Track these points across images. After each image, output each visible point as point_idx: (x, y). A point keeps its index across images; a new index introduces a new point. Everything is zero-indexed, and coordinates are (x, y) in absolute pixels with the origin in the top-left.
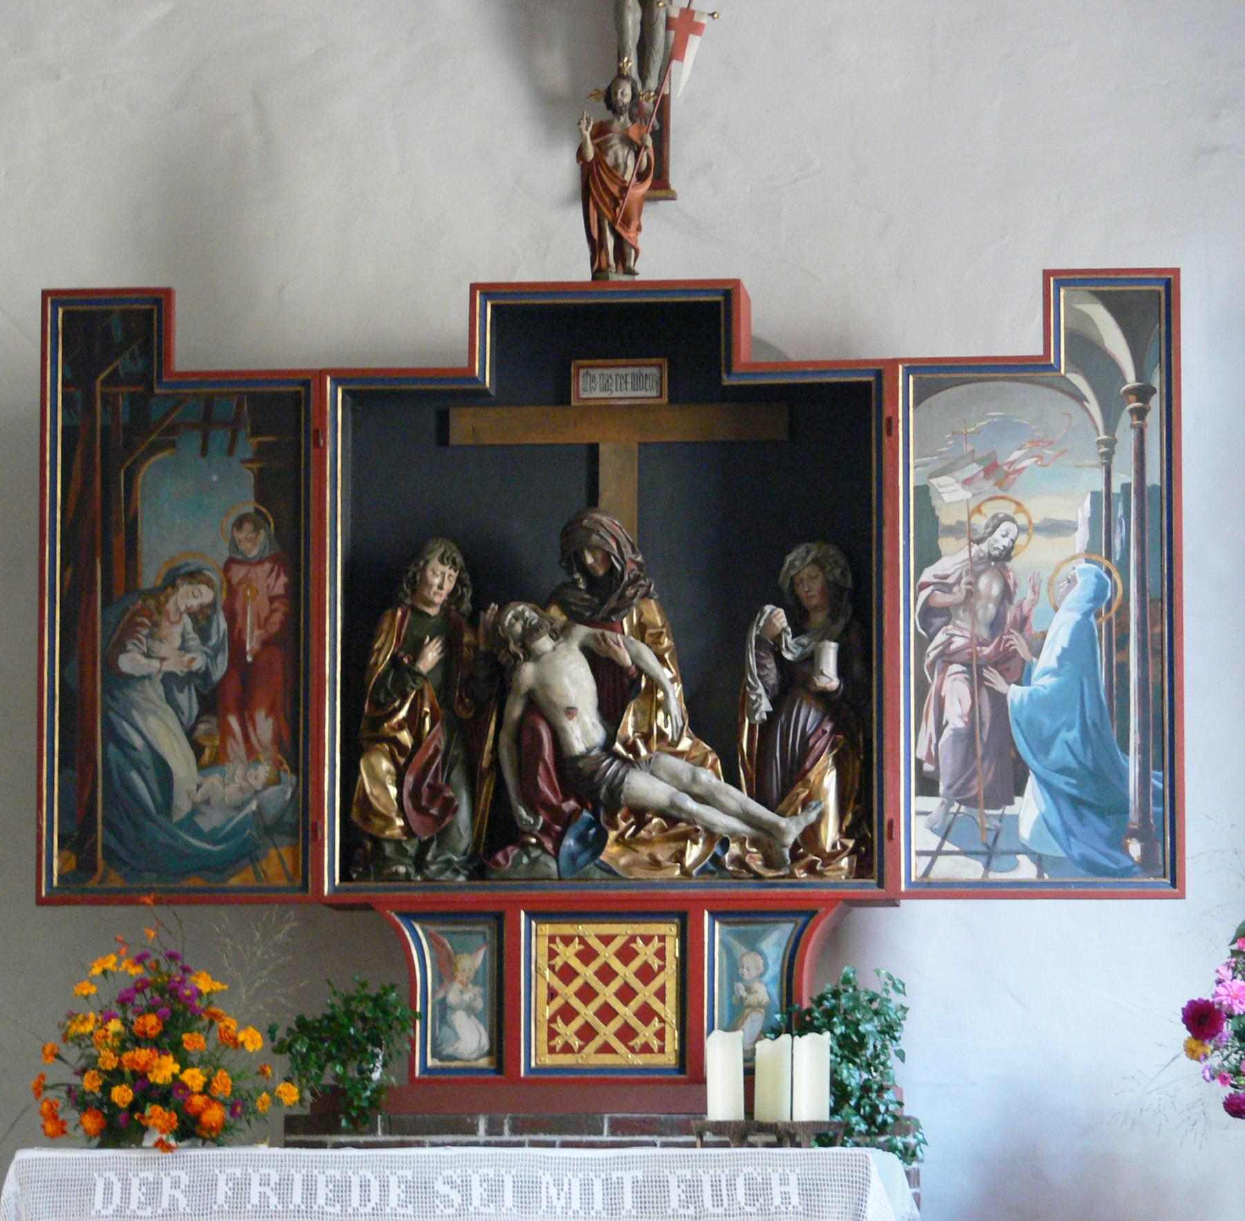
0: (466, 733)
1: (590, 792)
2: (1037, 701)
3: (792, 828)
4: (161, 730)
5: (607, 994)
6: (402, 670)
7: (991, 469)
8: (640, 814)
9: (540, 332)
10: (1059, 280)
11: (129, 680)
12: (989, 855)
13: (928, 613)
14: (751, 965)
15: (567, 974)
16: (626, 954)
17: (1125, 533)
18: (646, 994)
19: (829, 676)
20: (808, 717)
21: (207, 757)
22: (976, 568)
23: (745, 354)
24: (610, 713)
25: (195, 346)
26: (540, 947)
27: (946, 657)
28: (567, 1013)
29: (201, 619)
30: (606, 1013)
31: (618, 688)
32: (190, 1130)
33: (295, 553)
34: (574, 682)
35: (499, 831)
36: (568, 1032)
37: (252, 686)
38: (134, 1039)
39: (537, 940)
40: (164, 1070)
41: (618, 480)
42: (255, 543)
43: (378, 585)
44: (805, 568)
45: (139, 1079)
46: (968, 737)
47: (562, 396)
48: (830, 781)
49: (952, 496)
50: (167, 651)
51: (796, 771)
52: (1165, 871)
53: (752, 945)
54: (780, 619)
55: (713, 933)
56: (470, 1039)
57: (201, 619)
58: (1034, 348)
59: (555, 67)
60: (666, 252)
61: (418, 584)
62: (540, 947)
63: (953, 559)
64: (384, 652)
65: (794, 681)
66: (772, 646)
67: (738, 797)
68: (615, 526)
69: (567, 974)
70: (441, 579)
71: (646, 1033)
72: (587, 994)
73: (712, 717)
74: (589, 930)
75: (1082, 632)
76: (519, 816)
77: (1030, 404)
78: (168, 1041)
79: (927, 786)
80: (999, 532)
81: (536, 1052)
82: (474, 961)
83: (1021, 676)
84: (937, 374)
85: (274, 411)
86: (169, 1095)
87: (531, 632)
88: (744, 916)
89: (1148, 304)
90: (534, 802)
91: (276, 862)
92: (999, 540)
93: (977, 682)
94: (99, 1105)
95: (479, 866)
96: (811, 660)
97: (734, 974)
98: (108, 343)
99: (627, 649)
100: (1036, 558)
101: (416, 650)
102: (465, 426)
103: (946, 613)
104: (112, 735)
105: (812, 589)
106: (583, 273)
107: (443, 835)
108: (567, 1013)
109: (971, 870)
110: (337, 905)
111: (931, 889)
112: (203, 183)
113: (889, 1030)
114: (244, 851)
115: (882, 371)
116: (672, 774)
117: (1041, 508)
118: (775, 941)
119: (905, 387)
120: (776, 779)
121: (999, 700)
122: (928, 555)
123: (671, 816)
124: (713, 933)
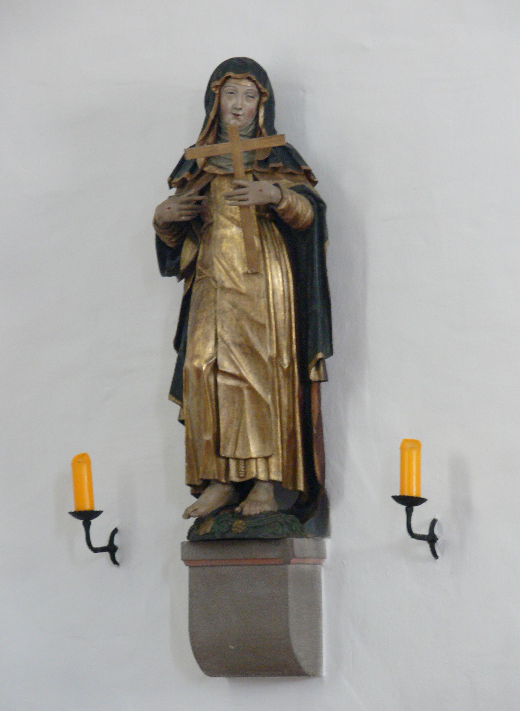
34: (277, 165)
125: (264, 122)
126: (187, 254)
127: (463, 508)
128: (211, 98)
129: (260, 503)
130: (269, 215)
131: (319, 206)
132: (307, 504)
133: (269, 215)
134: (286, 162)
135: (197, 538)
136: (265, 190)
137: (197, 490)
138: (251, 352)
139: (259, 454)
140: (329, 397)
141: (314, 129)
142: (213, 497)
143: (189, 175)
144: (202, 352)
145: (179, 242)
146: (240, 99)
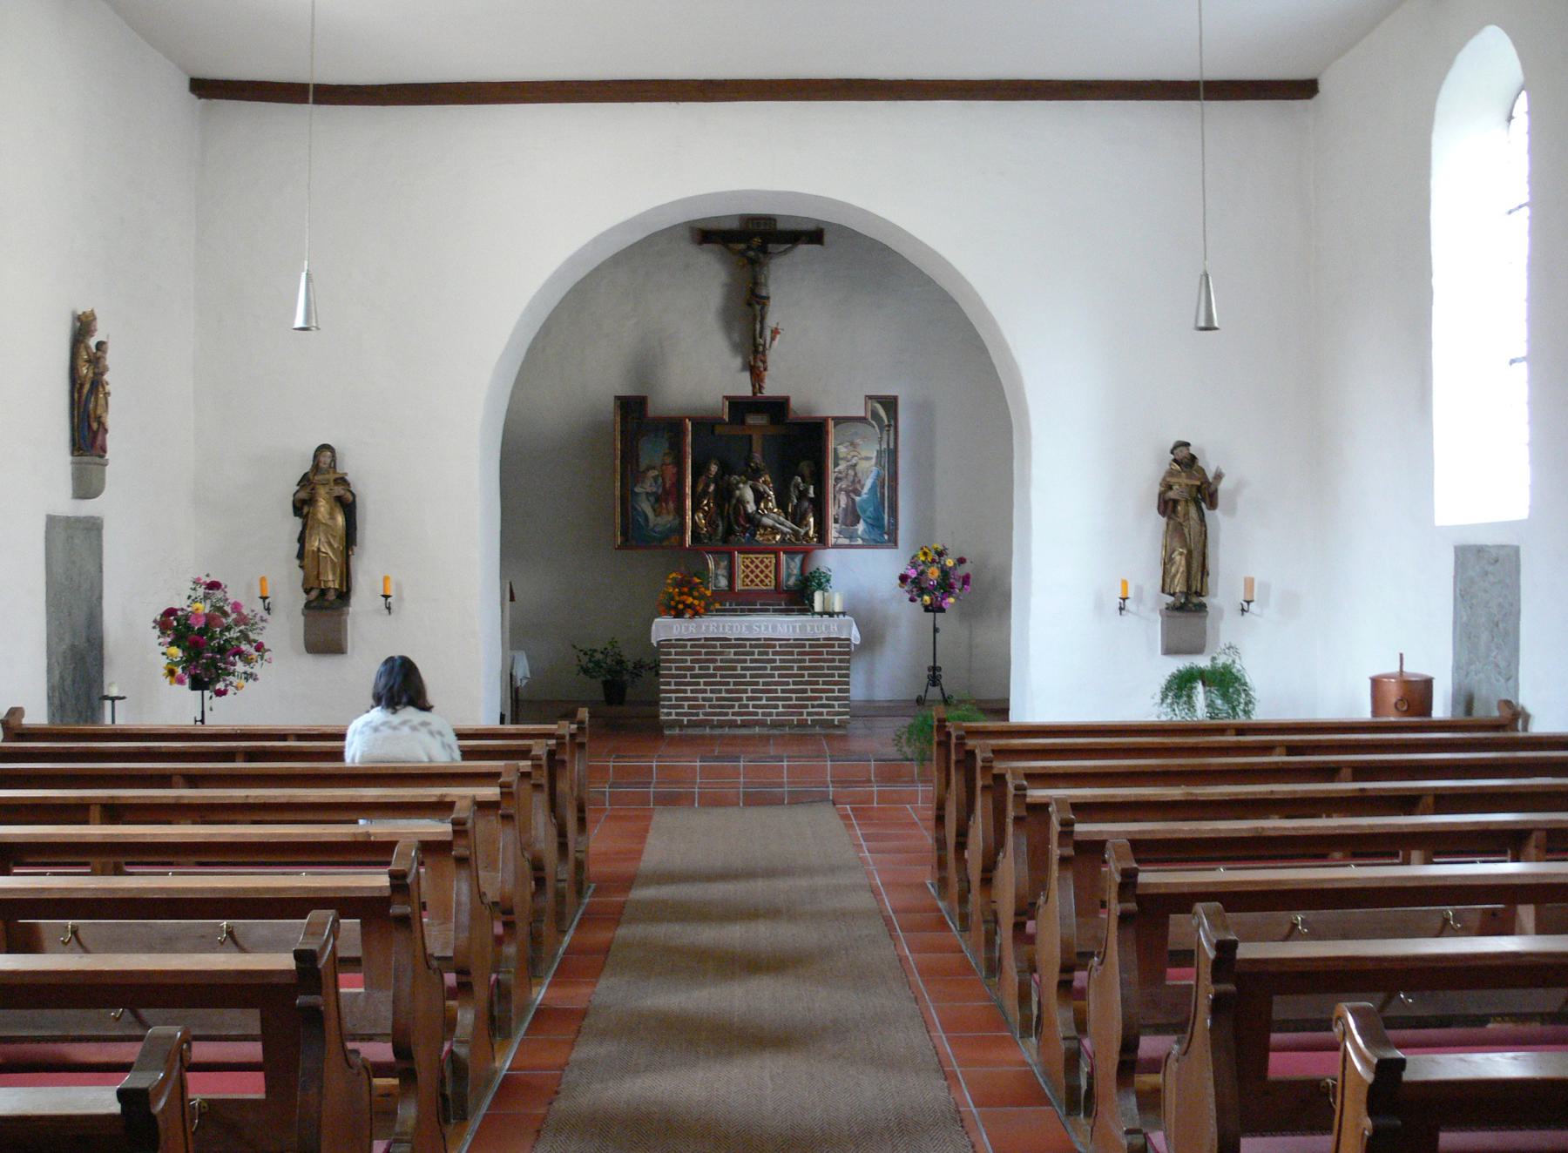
0: (719, 506)
1: (753, 522)
3: (802, 531)
4: (646, 506)
6: (705, 493)
7: (852, 444)
8: (765, 527)
9: (738, 406)
10: (870, 397)
11: (637, 494)
12: (851, 538)
13: (837, 480)
14: (792, 565)
17: (885, 460)
19: (811, 494)
20: (806, 504)
21: (657, 513)
22: (848, 468)
23: (792, 415)
24: (757, 503)
25: (652, 411)
29: (655, 478)
31: (759, 497)
32: (696, 614)
33: (680, 464)
34: (749, 495)
35: (729, 531)
38: (681, 594)
39: (739, 558)
40: (690, 600)
42: (669, 460)
44: (805, 466)
46: (845, 510)
49: (842, 450)
50: (647, 486)
52: (894, 542)
55: (783, 556)
56: (723, 582)
58: (862, 414)
59: (736, 337)
60: (771, 389)
64: (700, 487)
65: (802, 495)
66: (797, 486)
67: (789, 523)
68: (757, 457)
70: (714, 468)
73: (782, 504)
77: (860, 427)
79: (836, 521)
80: (854, 460)
81: (739, 586)
82: (724, 564)
84: (839, 421)
85: (672, 426)
88: (791, 553)
89: (890, 404)
91: (674, 540)
93: (848, 496)
95: (725, 540)
96: (807, 490)
100: (863, 465)
101: (708, 486)
102: (718, 430)
104: (634, 508)
105: (806, 471)
107: (715, 530)
109: (846, 542)
110: (690, 549)
111: (836, 546)
112: (645, 364)
114: (666, 535)
115: (826, 419)
116: (772, 516)
117: (864, 454)
118: (798, 559)
119: (831, 423)
120: (799, 519)
122: (836, 465)
123: (773, 528)
124: (783, 556)
125: (333, 465)
126: (305, 510)
127: (401, 599)
128: (316, 456)
129: (331, 596)
130: (339, 499)
131: (353, 495)
132: (344, 595)
133: (339, 499)
134: (342, 481)
135: (308, 606)
136: (339, 490)
137: (307, 591)
138: (330, 545)
139: (331, 580)
140: (353, 558)
141: (350, 466)
142: (314, 594)
143: (305, 481)
144: (314, 543)
145: (302, 506)
146: (326, 458)
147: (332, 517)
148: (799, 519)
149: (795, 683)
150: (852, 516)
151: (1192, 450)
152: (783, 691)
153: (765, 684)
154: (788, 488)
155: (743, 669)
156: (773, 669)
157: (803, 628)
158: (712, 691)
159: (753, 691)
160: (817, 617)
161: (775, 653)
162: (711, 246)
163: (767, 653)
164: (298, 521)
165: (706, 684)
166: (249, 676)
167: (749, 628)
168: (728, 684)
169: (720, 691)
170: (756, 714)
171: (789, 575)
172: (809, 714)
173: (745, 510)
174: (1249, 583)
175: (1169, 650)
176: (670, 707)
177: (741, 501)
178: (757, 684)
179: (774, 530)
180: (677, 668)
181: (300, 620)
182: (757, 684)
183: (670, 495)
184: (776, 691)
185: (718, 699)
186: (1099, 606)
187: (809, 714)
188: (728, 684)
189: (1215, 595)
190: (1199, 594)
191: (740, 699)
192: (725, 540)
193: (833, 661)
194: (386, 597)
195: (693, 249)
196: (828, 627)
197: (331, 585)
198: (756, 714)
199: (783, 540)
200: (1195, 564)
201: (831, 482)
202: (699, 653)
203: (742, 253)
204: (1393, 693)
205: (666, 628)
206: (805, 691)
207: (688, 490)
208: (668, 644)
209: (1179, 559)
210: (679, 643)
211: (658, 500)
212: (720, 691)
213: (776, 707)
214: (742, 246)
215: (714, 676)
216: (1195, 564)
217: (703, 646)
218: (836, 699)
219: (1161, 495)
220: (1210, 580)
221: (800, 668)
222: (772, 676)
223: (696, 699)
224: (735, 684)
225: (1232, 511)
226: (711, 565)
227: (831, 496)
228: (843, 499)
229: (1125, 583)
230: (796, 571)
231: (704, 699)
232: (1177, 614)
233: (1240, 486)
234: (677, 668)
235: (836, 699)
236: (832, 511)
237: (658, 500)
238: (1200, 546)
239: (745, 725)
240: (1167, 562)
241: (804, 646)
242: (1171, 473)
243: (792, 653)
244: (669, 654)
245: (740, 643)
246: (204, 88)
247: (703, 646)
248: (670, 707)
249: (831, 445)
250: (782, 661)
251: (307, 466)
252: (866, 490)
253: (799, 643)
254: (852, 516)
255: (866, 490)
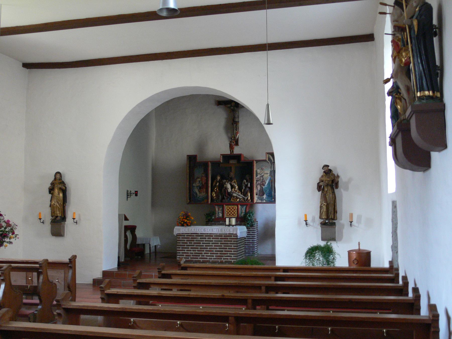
1: (230, 195)
2: (265, 188)
3: (246, 198)
4: (196, 190)
5: (231, 211)
7: (262, 169)
8: (234, 197)
9: (226, 157)
10: (268, 153)
12: (262, 200)
13: (257, 181)
14: (243, 209)
15: (228, 210)
16: (233, 208)
18: (234, 211)
20: (247, 189)
24: (232, 189)
25: (198, 159)
26: (226, 208)
27: (258, 184)
28: (228, 213)
29: (199, 182)
30: (231, 213)
31: (232, 187)
32: (188, 225)
34: (229, 186)
35: (223, 198)
36: (228, 214)
37: (204, 187)
39: (226, 207)
40: (186, 221)
41: (233, 170)
42: (203, 175)
43: (213, 178)
45: (184, 221)
46: (260, 191)
47: (229, 163)
48: (249, 194)
49: (259, 171)
51: (247, 193)
53: (243, 207)
54: (245, 181)
55: (239, 206)
56: (221, 215)
57: (199, 182)
59: (230, 135)
60: (237, 151)
61: (217, 178)
62: (226, 208)
63: (259, 176)
65: (246, 186)
66: (244, 183)
67: (241, 195)
68: (232, 174)
69: (228, 210)
70: (219, 178)
71: (234, 214)
72: (230, 211)
73: (240, 189)
74: (230, 206)
75: (269, 182)
76: (224, 198)
77: (264, 163)
78: (186, 219)
82: (221, 209)
83: (264, 186)
84: (258, 161)
85: (205, 165)
86: (186, 223)
87: (225, 182)
90: (226, 196)
92: (262, 175)
93: (261, 186)
94: (181, 223)
95: (221, 201)
96: (248, 184)
97: (241, 209)
98: (192, 159)
99: (233, 184)
100: (265, 176)
103: (258, 181)
105: (248, 179)
106: (229, 153)
107: (218, 199)
108: (228, 213)
109: (260, 201)
111: (257, 203)
112: (201, 146)
113: (253, 214)
116: (237, 194)
117: (266, 172)
118: (245, 207)
119: (255, 162)
120: (245, 194)
121: (262, 188)
122: (257, 176)
123: (236, 197)
124: (239, 206)
125: (61, 179)
126: (52, 192)
128: (55, 176)
130: (60, 189)
131: (66, 188)
132: (64, 218)
133: (60, 189)
134: (63, 183)
137: (52, 216)
138: (58, 203)
139: (59, 214)
140: (66, 207)
141: (66, 179)
142: (54, 218)
143: (52, 184)
145: (51, 190)
146: (58, 176)
147: (59, 194)
148: (245, 194)
149: (219, 249)
150: (262, 193)
151: (329, 168)
152: (215, 251)
153: (210, 248)
154: (242, 184)
155: (203, 243)
156: (212, 243)
157: (221, 230)
158: (193, 251)
159: (206, 251)
160: (227, 227)
161: (213, 238)
162: (221, 106)
163: (210, 238)
164: (50, 195)
165: (191, 248)
166: (11, 243)
167: (204, 230)
168: (198, 248)
169: (195, 251)
170: (207, 258)
171: (242, 212)
172: (224, 259)
173: (228, 191)
174: (351, 215)
175: (323, 239)
176: (179, 255)
177: (226, 189)
178: (207, 248)
179: (237, 198)
180: (182, 243)
181: (50, 225)
182: (207, 248)
183: (204, 187)
184: (213, 251)
185: (195, 253)
186: (299, 223)
187: (224, 259)
188: (198, 248)
189: (341, 220)
190: (334, 219)
191: (202, 253)
192: (221, 201)
193: (232, 241)
194: (74, 219)
195: (216, 107)
196: (229, 230)
197: (59, 215)
198: (207, 258)
199: (240, 201)
200: (331, 209)
201: (255, 182)
202: (189, 238)
203: (229, 107)
204: (354, 256)
205: (179, 230)
206: (222, 251)
207: (210, 185)
208: (179, 235)
209: (325, 207)
210: (183, 235)
211: (200, 188)
212: (195, 251)
213: (213, 256)
214: (229, 106)
215: (194, 246)
216: (331, 209)
217: (228, 236)
218: (233, 254)
219: (318, 184)
220: (338, 215)
221: (221, 244)
222: (212, 246)
223: (188, 253)
224: (200, 248)
225: (347, 189)
226: (217, 209)
227: (255, 186)
228: (259, 187)
229: (306, 215)
230: (244, 211)
231: (190, 253)
232: (325, 226)
233: (350, 180)
234: (182, 243)
235: (233, 254)
236: (255, 191)
237: (200, 188)
238: (332, 202)
239: (204, 262)
240: (321, 207)
241: (222, 236)
242: (322, 176)
243: (218, 238)
244: (180, 238)
245: (201, 235)
246: (27, 66)
247: (228, 236)
248: (179, 255)
249: (255, 170)
250: (215, 241)
251: (52, 178)
252: (266, 184)
253: (220, 235)
254: (262, 193)
255: (266, 184)
